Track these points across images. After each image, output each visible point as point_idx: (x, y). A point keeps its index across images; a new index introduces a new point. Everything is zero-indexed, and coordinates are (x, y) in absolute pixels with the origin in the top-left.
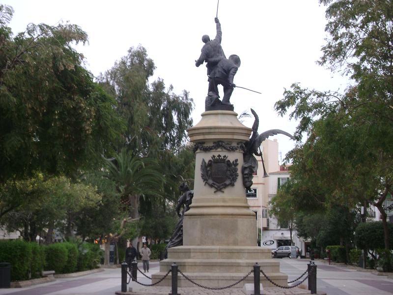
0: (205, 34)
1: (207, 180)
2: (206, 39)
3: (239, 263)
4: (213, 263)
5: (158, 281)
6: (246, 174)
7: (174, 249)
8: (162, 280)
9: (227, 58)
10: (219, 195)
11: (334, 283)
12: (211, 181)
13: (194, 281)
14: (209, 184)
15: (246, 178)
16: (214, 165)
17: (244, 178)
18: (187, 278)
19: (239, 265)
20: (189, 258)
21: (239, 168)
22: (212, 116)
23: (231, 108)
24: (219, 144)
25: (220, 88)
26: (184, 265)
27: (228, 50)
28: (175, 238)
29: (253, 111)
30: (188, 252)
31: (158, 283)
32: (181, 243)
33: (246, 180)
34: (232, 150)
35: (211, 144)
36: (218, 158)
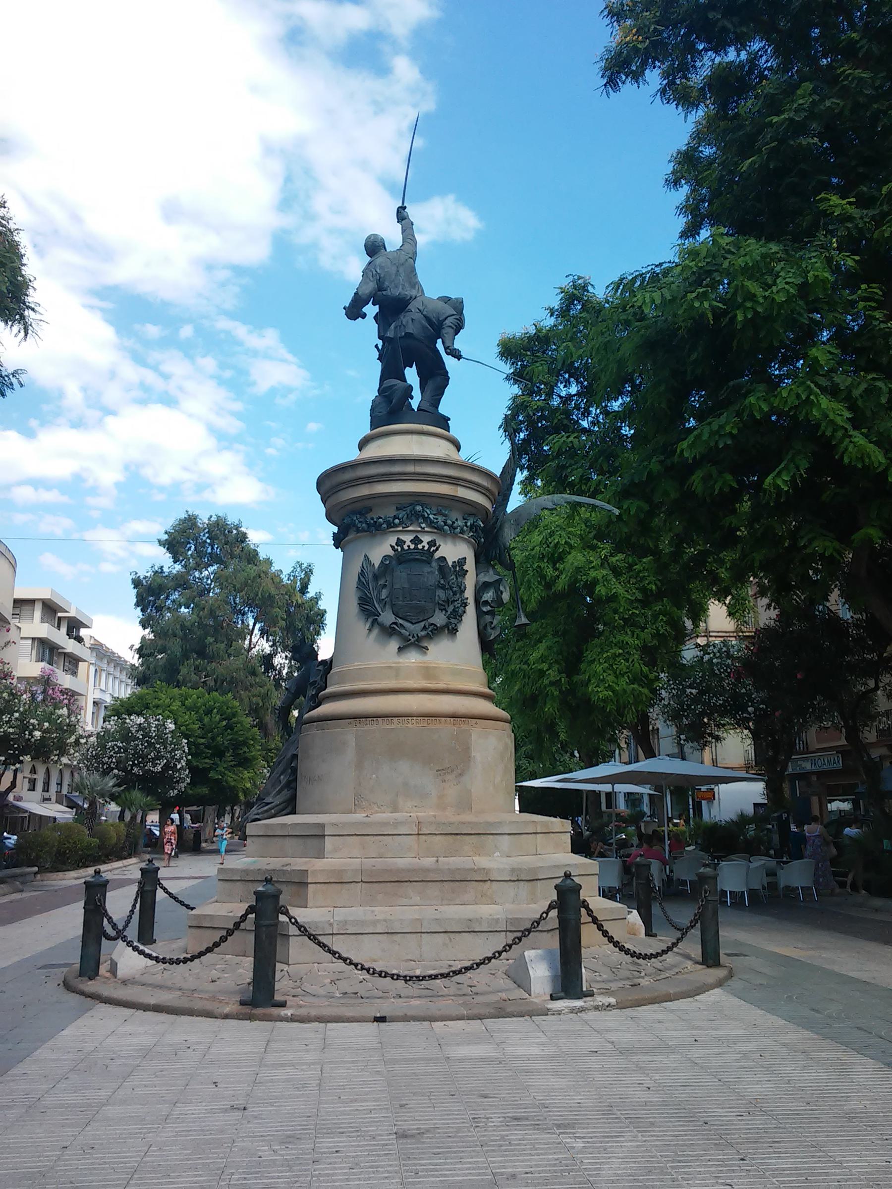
2: (374, 247)
3: (487, 871)
4: (399, 871)
5: (216, 936)
6: (486, 603)
7: (267, 825)
8: (230, 932)
9: (450, 564)
10: (413, 658)
11: (726, 934)
12: (387, 617)
13: (337, 944)
14: (382, 627)
15: (488, 613)
16: (401, 576)
17: (480, 614)
18: (303, 930)
19: (485, 879)
20: (320, 855)
21: (470, 582)
23: (444, 422)
24: (413, 509)
25: (412, 375)
26: (301, 883)
27: (434, 284)
28: (403, 631)
30: (317, 835)
31: (216, 945)
32: (291, 806)
33: (488, 618)
34: (453, 533)
35: (390, 512)
36: (412, 546)
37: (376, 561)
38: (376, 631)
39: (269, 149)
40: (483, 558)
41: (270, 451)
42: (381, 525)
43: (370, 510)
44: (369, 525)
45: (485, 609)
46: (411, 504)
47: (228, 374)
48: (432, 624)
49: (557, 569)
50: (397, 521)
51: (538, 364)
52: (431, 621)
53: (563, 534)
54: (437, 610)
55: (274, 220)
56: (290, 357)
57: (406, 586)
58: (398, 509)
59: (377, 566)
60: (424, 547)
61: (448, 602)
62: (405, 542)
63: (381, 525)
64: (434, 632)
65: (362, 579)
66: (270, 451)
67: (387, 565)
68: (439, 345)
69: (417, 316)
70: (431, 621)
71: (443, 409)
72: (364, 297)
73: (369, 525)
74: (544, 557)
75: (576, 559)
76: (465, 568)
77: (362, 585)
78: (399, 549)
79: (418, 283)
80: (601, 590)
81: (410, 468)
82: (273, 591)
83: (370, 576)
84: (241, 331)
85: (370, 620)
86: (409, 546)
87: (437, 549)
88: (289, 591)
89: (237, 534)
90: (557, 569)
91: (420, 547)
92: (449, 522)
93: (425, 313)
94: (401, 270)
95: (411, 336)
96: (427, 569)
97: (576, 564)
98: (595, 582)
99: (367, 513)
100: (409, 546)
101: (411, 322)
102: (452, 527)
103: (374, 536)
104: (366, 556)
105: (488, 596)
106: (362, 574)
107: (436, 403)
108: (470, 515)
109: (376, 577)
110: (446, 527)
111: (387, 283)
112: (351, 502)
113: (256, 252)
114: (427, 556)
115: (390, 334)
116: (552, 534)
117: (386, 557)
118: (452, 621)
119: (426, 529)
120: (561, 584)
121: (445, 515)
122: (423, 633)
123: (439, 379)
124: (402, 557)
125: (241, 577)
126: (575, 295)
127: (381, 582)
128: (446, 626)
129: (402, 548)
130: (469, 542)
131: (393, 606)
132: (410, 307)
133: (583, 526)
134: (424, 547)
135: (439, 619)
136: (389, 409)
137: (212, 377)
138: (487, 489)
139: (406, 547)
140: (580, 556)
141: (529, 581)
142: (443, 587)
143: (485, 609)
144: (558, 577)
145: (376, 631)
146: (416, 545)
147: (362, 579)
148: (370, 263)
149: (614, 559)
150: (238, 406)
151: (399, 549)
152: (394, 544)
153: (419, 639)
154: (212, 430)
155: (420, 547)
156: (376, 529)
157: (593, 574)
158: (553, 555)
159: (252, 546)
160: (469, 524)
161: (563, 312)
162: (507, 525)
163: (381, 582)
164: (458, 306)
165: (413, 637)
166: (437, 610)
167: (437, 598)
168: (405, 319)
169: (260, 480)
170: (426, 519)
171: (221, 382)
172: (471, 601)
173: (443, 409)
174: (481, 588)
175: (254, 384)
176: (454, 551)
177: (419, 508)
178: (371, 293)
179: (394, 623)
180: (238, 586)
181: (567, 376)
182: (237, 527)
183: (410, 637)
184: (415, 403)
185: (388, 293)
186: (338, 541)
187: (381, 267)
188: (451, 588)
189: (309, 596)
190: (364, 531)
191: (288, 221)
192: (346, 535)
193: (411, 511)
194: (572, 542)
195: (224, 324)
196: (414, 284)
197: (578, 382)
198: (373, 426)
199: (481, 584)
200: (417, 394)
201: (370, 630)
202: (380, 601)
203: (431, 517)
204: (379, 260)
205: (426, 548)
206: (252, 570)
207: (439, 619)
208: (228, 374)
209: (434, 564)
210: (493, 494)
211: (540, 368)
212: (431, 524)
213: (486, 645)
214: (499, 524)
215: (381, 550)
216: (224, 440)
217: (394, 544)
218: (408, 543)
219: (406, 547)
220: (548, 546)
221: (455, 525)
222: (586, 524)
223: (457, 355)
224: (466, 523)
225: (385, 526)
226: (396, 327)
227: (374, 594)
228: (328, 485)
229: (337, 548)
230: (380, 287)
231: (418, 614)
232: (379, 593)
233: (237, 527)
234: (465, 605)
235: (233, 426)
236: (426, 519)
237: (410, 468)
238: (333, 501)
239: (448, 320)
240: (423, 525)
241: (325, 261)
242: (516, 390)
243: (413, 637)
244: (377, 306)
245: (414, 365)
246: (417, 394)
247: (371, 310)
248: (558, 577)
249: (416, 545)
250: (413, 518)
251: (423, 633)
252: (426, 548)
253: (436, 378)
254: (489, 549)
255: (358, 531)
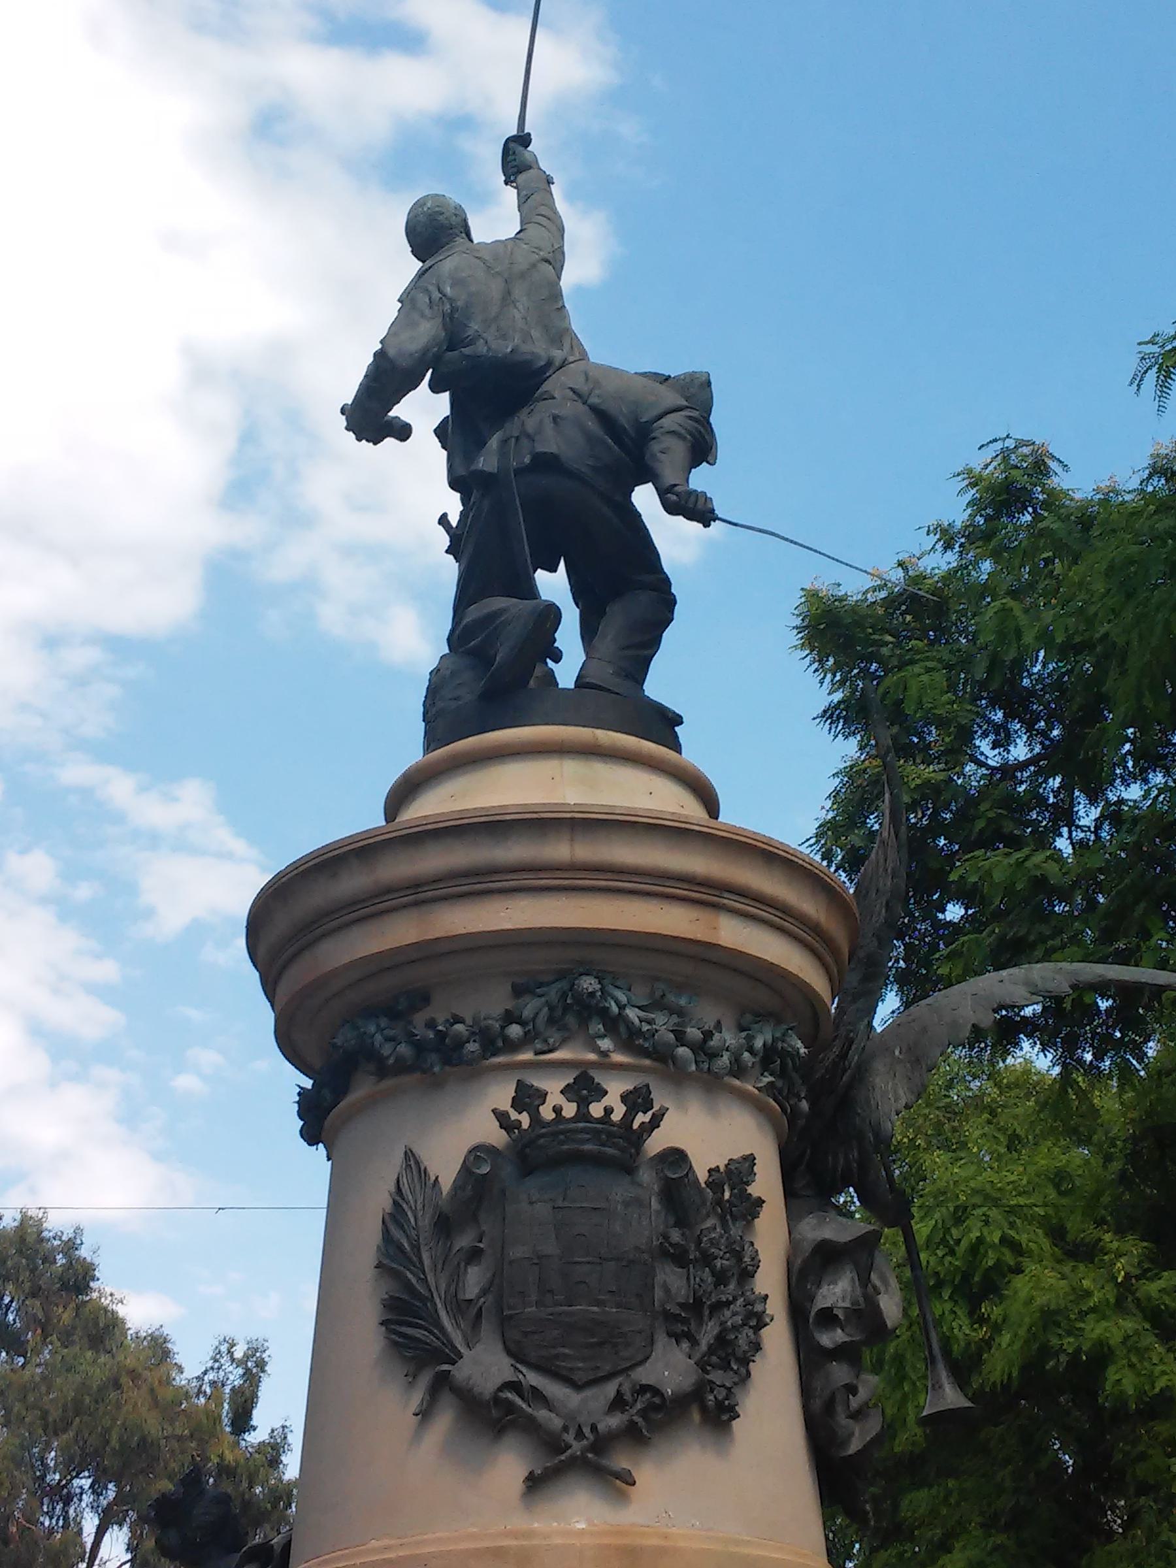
0: (682, 1147)
1: (454, 1357)
6: (828, 1318)
9: (702, 1176)
12: (486, 1365)
15: (840, 1353)
16: (533, 1203)
17: (810, 1360)
21: (771, 1238)
22: (522, 895)
23: (663, 724)
24: (568, 986)
28: (542, 1414)
29: (1139, 344)
33: (840, 1373)
34: (708, 1074)
35: (491, 1003)
36: (570, 1110)
37: (445, 1162)
38: (444, 1420)
39: (202, 371)
40: (807, 1181)
41: (186, 1082)
42: (460, 1043)
43: (423, 998)
44: (420, 1047)
45: (828, 1339)
46: (561, 975)
47: (84, 892)
48: (644, 1389)
49: (982, 1320)
50: (515, 1030)
51: (917, 669)
52: (644, 1375)
53: (994, 1213)
54: (662, 1340)
55: (214, 530)
56: (239, 846)
57: (551, 1248)
58: (519, 991)
59: (447, 1183)
60: (608, 1111)
61: (696, 1307)
62: (543, 1096)
63: (460, 1043)
64: (654, 1418)
65: (397, 1233)
66: (186, 1082)
67: (481, 1181)
68: (645, 498)
69: (571, 409)
70: (644, 1375)
71: (660, 685)
72: (404, 363)
73: (420, 1047)
74: (940, 1284)
75: (1041, 1283)
76: (754, 1190)
77: (395, 1257)
78: (525, 1119)
79: (568, 331)
80: (1121, 1380)
81: (560, 850)
82: (153, 1425)
83: (426, 1222)
84: (120, 788)
85: (425, 1379)
86: (557, 1110)
87: (655, 1122)
88: (203, 1429)
89: (70, 1265)
90: (982, 1320)
91: (596, 1110)
92: (693, 1033)
93: (594, 400)
94: (518, 291)
95: (552, 474)
96: (619, 1190)
97: (1041, 1300)
98: (1102, 1356)
99: (414, 1008)
100: (557, 1110)
101: (551, 427)
102: (703, 1049)
103: (437, 1084)
104: (409, 1155)
105: (836, 1292)
106: (396, 1216)
107: (638, 669)
108: (763, 1016)
109: (444, 1225)
110: (683, 1051)
111: (474, 326)
112: (358, 984)
113: (165, 604)
114: (618, 1147)
115: (487, 462)
116: (960, 1215)
117: (479, 1152)
118: (717, 1376)
119: (618, 1058)
120: (1000, 1364)
121: (680, 1012)
122: (614, 1421)
123: (643, 600)
124: (536, 1151)
125: (65, 1388)
126: (1012, 492)
127: (464, 1241)
128: (696, 1395)
129: (536, 1118)
130: (760, 1108)
131: (504, 1323)
132: (546, 387)
133: (1052, 1194)
134: (608, 1111)
135: (670, 1368)
136: (487, 682)
137: (44, 900)
138: (815, 929)
139: (547, 1113)
140: (1050, 1277)
141: (899, 1359)
142: (679, 1258)
143: (828, 1339)
144: (987, 1344)
145: (444, 1420)
146: (583, 1104)
147: (397, 1233)
148: (421, 274)
149: (1152, 1288)
150: (107, 971)
151: (525, 1119)
152: (505, 1105)
153: (602, 1444)
154: (38, 1031)
155: (596, 1110)
156: (447, 1060)
157: (1095, 1330)
158: (966, 1277)
159: (105, 1302)
160: (759, 1043)
161: (976, 537)
162: (880, 1066)
163: (464, 1241)
164: (696, 394)
165: (580, 1435)
166: (662, 1340)
167: (659, 1294)
168: (533, 419)
169: (157, 1156)
170: (614, 1024)
171: (65, 911)
172: (777, 1308)
173: (660, 685)
174: (810, 1266)
175: (149, 913)
176: (712, 1132)
177: (589, 984)
178: (425, 351)
179: (514, 1386)
180: (55, 1414)
181: (998, 716)
182: (70, 1246)
183: (569, 1437)
184: (566, 673)
185: (481, 348)
186: (317, 1120)
187: (457, 282)
188: (707, 1259)
189: (254, 1438)
190: (402, 1068)
191: (243, 530)
192: (341, 1091)
193: (564, 996)
194: (1023, 1238)
195: (77, 772)
196: (561, 334)
197: (1030, 728)
198: (432, 740)
199: (807, 1248)
200: (568, 634)
201: (425, 1414)
202: (459, 1306)
203: (632, 1014)
204: (449, 263)
205: (616, 1117)
206: (95, 1367)
207: (670, 1368)
208: (84, 892)
209: (646, 1176)
210: (834, 950)
211: (925, 678)
212: (630, 1039)
213: (838, 1478)
214: (854, 1057)
215: (461, 1128)
216: (67, 1056)
217: (505, 1105)
218: (555, 1098)
219: (547, 1113)
220: (952, 1252)
221: (714, 1042)
222: (1057, 1186)
223: (699, 511)
224: (749, 1039)
225: (472, 1047)
226: (504, 442)
227: (438, 1283)
228: (281, 924)
229: (311, 1135)
230: (454, 334)
231: (599, 1351)
232: (457, 1278)
233: (70, 1246)
234: (759, 1321)
235: (91, 1019)
236: (614, 1024)
237: (560, 850)
238: (294, 979)
239: (667, 431)
240: (605, 1044)
241: (331, 617)
242: (849, 749)
243: (580, 1435)
244: (446, 396)
245: (562, 565)
246: (568, 634)
247: (424, 408)
248: (987, 1344)
249: (583, 1104)
250: (571, 1020)
251: (614, 1421)
252: (616, 1117)
253: (632, 596)
254: (828, 1144)
255: (383, 1071)
